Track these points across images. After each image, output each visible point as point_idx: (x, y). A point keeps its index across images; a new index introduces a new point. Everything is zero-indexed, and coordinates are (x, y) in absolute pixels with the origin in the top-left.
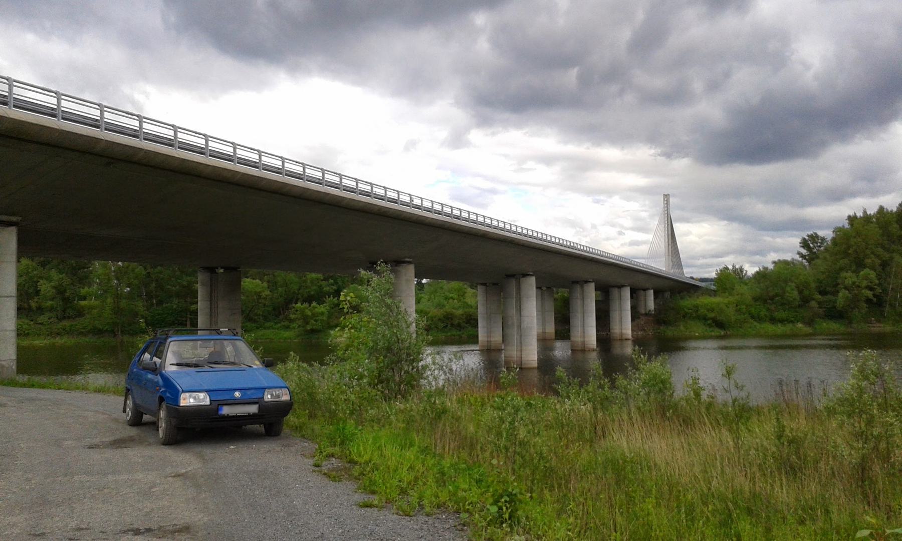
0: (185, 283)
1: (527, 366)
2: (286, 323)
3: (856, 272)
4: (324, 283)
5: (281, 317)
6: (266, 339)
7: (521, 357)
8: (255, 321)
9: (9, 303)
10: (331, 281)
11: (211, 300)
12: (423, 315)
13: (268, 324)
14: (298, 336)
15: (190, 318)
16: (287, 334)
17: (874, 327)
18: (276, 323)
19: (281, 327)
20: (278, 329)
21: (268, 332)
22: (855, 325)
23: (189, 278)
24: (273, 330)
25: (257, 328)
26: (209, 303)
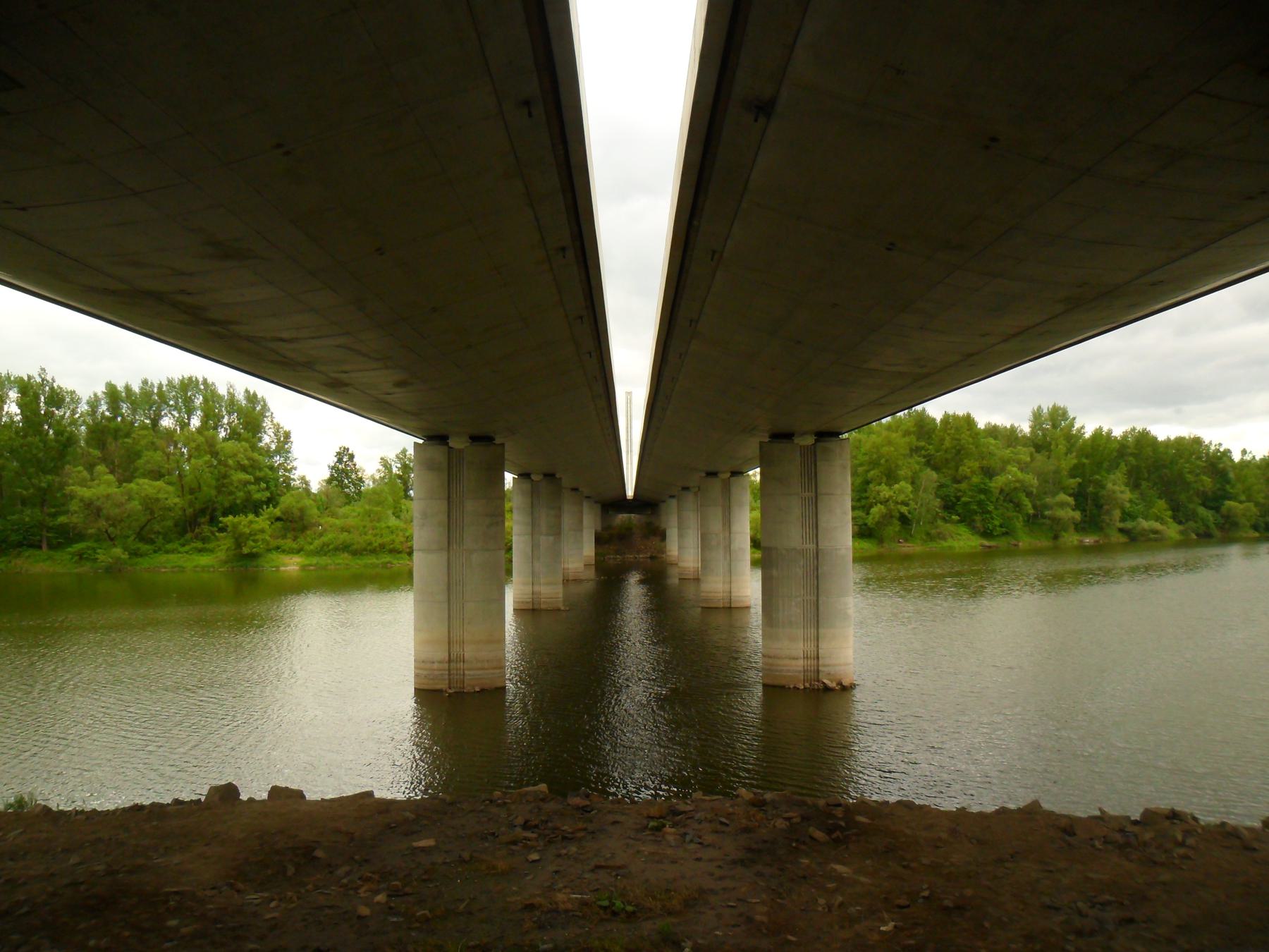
0: (43, 485)
1: (738, 605)
2: (199, 545)
3: (889, 485)
4: (252, 488)
5: (189, 535)
6: (173, 567)
7: (730, 592)
8: (152, 542)
9: (353, 477)
10: (263, 485)
11: (449, 497)
12: (252, 533)
13: (169, 546)
14: (226, 562)
15: (48, 538)
16: (204, 560)
17: (904, 547)
18: (183, 545)
19: (191, 550)
20: (187, 552)
21: (171, 556)
22: (886, 545)
23: (49, 477)
24: (180, 555)
25: (155, 552)
26: (446, 502)
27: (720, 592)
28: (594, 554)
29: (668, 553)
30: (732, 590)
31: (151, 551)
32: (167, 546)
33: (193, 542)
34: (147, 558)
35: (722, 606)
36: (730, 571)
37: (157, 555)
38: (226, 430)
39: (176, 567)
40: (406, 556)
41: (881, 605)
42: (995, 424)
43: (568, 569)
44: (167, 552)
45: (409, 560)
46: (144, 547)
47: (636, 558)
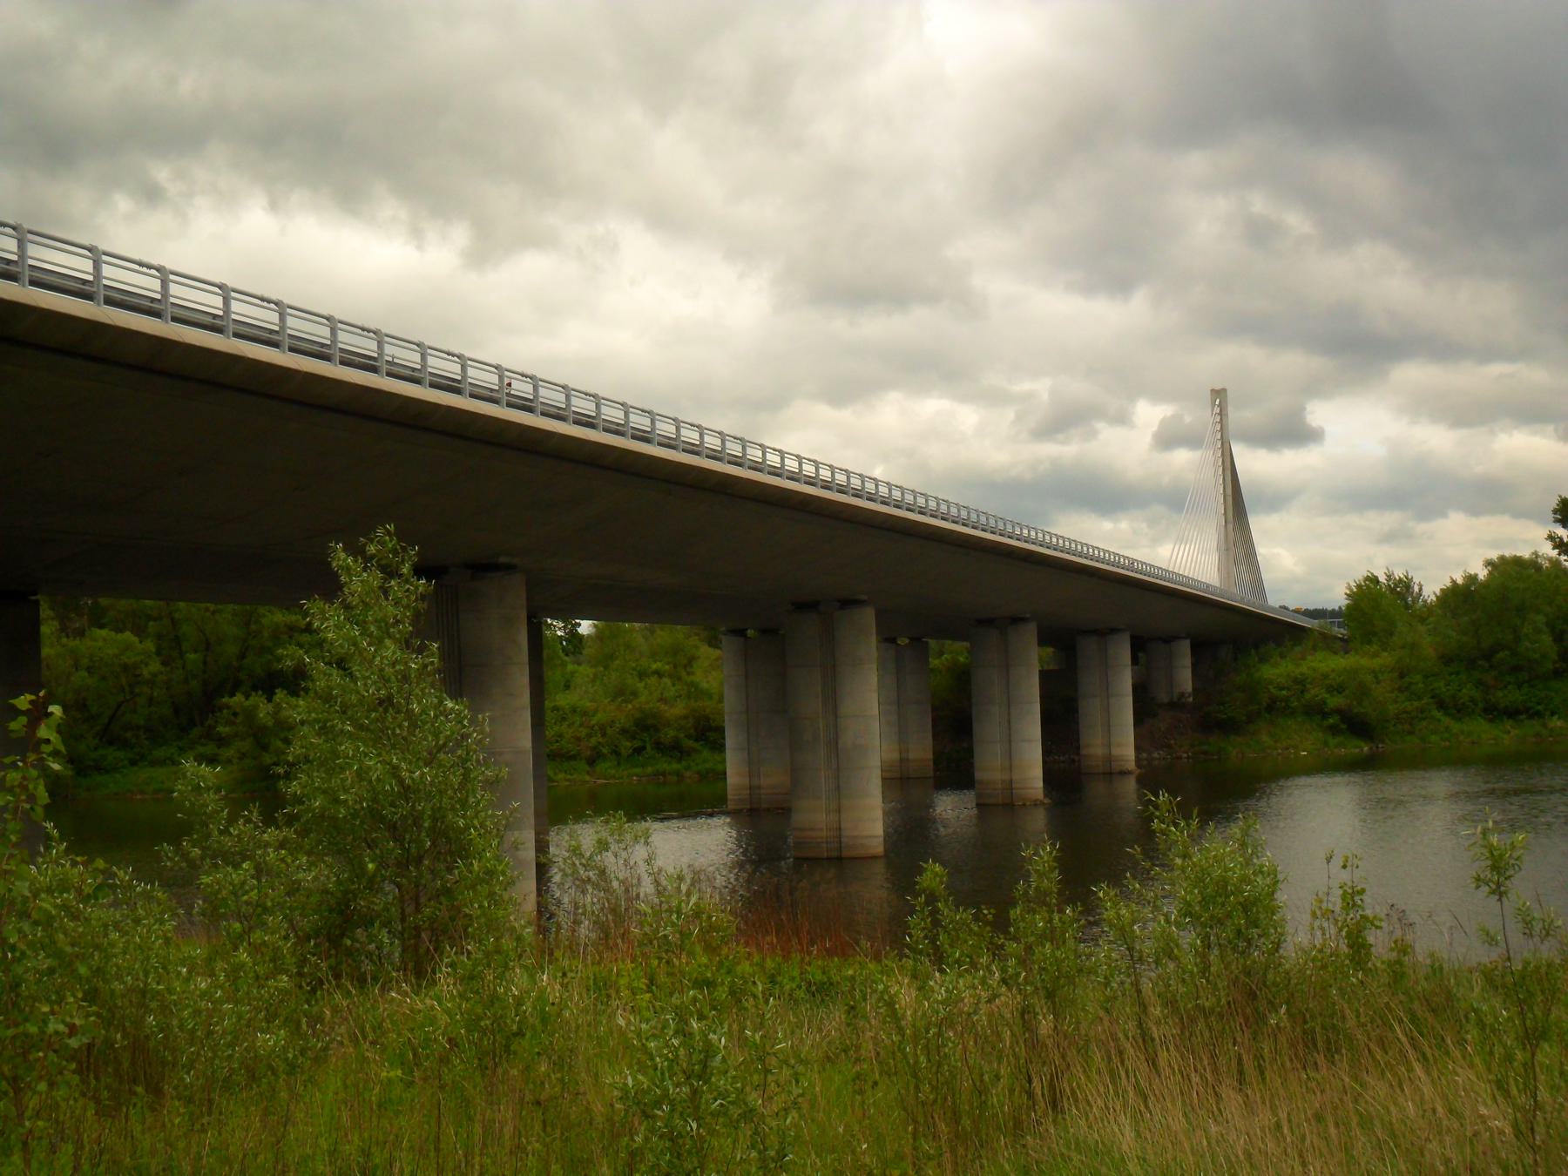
13: (160, 753)
25: (133, 763)
27: (821, 829)
28: (930, 755)
29: (1084, 752)
30: (842, 826)
31: (126, 762)
32: (154, 752)
33: (203, 745)
34: (118, 775)
35: (825, 855)
36: (838, 788)
37: (135, 768)
38: (315, 879)
39: (1513, 713)
40: (583, 766)
41: (462, 785)
42: (1441, 590)
43: (759, 787)
44: (154, 763)
45: (588, 773)
46: (112, 754)
47: (1073, 761)
